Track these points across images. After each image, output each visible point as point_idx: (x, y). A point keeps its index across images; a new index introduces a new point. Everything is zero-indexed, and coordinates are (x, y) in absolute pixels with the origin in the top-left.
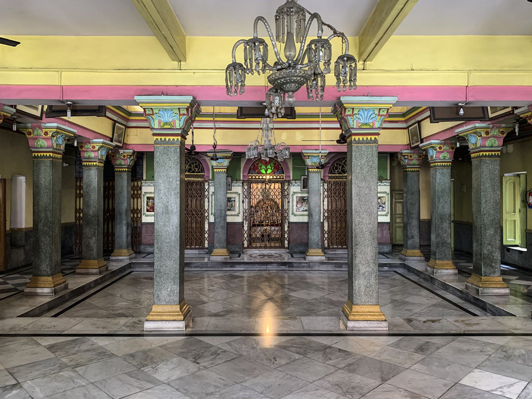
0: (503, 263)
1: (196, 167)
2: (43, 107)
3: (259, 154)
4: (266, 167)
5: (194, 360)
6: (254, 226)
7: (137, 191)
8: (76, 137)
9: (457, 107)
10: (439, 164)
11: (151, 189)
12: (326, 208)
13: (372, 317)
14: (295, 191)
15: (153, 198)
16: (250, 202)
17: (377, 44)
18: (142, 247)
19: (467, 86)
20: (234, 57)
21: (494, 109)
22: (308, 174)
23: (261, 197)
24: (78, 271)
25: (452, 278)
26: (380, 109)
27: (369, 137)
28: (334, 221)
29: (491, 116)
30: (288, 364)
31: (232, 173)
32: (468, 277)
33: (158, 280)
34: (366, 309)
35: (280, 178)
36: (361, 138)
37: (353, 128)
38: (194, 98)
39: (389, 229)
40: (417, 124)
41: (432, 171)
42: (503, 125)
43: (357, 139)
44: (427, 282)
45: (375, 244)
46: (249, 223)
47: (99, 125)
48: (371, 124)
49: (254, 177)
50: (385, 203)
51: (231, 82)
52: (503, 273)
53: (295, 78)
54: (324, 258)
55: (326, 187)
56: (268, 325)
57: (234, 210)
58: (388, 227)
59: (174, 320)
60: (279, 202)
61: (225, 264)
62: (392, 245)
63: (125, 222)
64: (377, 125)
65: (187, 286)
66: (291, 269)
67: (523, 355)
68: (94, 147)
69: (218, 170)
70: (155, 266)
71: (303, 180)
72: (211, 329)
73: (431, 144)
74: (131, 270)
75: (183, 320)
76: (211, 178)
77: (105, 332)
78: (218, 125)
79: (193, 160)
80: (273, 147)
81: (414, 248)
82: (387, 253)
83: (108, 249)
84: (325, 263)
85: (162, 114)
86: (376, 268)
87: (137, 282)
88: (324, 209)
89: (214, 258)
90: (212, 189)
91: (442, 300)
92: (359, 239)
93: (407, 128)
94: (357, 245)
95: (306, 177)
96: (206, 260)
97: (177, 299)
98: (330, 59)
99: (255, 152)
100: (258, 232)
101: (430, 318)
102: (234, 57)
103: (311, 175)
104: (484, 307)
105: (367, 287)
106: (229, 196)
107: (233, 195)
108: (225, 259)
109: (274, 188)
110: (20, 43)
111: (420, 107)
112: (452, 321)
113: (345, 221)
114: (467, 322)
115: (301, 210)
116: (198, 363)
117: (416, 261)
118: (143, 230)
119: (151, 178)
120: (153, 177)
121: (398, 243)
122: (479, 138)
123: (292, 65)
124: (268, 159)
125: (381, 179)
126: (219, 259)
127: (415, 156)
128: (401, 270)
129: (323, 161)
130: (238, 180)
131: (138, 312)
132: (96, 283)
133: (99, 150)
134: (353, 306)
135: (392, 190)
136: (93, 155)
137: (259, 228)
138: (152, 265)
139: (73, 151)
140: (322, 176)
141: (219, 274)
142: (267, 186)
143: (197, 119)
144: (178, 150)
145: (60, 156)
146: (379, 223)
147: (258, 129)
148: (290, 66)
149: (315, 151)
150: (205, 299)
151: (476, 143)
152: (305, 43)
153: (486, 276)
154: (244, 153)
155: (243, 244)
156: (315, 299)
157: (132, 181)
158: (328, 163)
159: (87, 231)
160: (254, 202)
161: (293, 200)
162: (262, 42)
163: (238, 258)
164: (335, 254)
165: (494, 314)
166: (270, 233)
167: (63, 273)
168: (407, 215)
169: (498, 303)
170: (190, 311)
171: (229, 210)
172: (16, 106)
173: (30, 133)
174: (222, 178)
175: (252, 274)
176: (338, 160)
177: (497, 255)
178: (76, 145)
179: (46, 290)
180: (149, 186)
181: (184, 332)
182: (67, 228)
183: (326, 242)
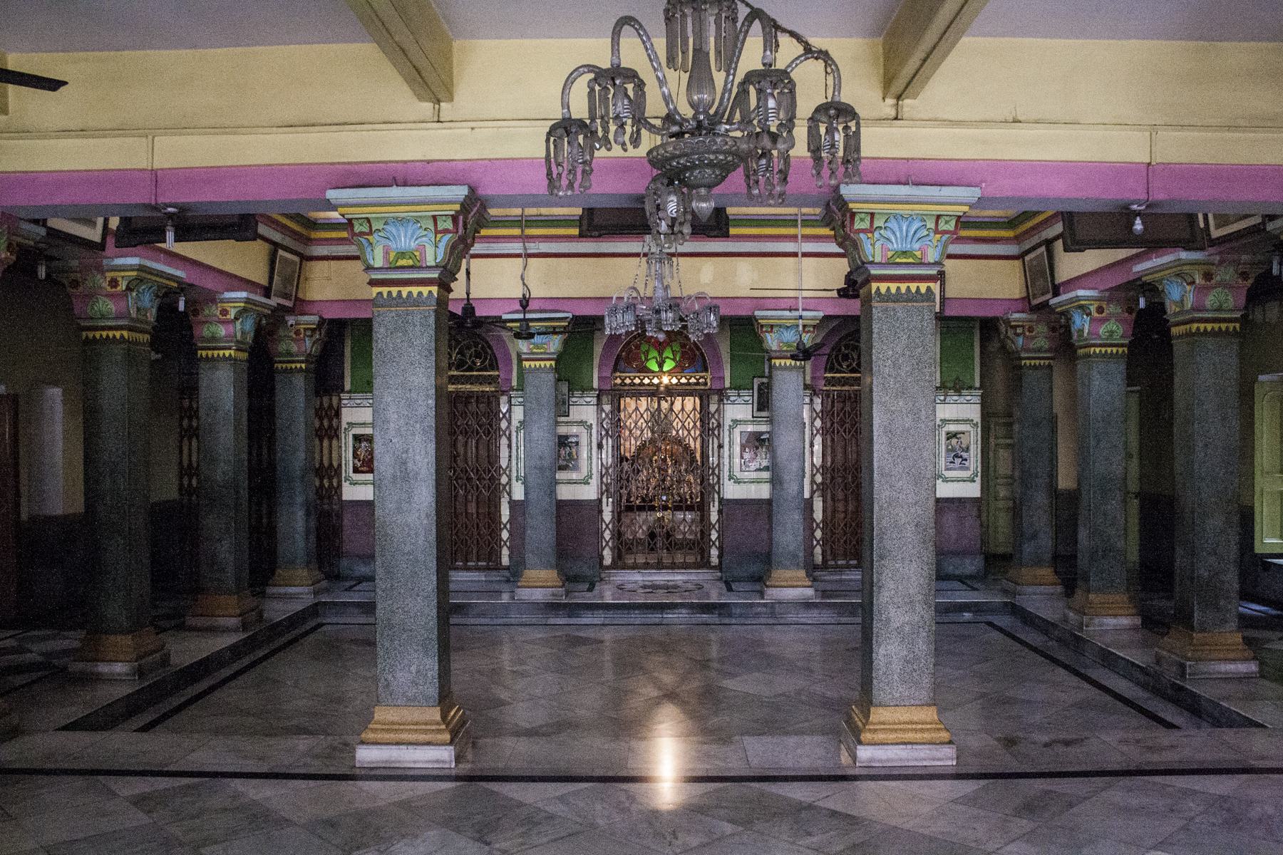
0: (1246, 596)
1: (478, 355)
2: (106, 220)
3: (641, 323)
4: (660, 354)
5: (478, 835)
6: (630, 508)
7: (330, 420)
8: (184, 288)
9: (1125, 214)
10: (1097, 350)
11: (365, 415)
12: (818, 461)
13: (919, 736)
14: (739, 417)
15: (369, 439)
16: (617, 447)
17: (925, 60)
18: (344, 563)
19: (1149, 164)
20: (565, 105)
21: (1223, 220)
22: (770, 372)
23: (648, 434)
24: (191, 621)
25: (1125, 637)
26: (938, 217)
27: (913, 286)
28: (840, 495)
29: (1215, 233)
30: (703, 845)
31: (569, 371)
32: (1163, 635)
33: (387, 644)
34: (902, 715)
35: (697, 384)
36: (893, 287)
37: (872, 263)
38: (472, 190)
39: (979, 516)
40: (1043, 249)
41: (1081, 367)
42: (1244, 257)
43: (883, 290)
44: (1067, 650)
45: (929, 555)
46: (617, 504)
47: (240, 259)
48: (918, 254)
49: (628, 381)
50: (967, 450)
51: (558, 165)
52: (1247, 622)
53: (712, 157)
54: (810, 592)
55: (818, 408)
56: (667, 762)
57: (576, 468)
58: (975, 513)
59: (428, 743)
60: (695, 445)
61: (552, 607)
62: (977, 555)
63: (299, 499)
64: (932, 256)
65: (457, 663)
66: (727, 621)
67: (1270, 817)
68: (224, 312)
69: (533, 363)
70: (380, 612)
71: (759, 389)
72: (516, 767)
73: (1078, 298)
74: (319, 620)
75: (451, 743)
76: (514, 383)
77: (265, 769)
78: (533, 247)
79: (469, 338)
80: (674, 304)
81: (1038, 563)
82: (971, 577)
83: (262, 568)
84: (815, 605)
85: (394, 231)
86: (929, 615)
87: (333, 650)
88: (813, 464)
89: (525, 594)
90: (518, 414)
91: (1097, 691)
92: (888, 543)
93: (1021, 257)
94: (882, 557)
95: (765, 380)
96: (505, 598)
97: (433, 691)
98: (793, 116)
99: (629, 318)
100: (641, 523)
101: (1063, 736)
102: (565, 105)
103: (778, 375)
104: (1196, 708)
105: (908, 662)
106: (562, 430)
107: (574, 430)
108: (553, 595)
109: (683, 409)
110: (65, 83)
111: (1038, 213)
112: (1114, 741)
113: (858, 498)
114: (1150, 744)
115: (753, 468)
116: (488, 844)
117: (1041, 597)
118: (346, 522)
119: (365, 386)
120: (370, 383)
121: (1001, 550)
122: (1188, 288)
123: (705, 126)
124: (661, 337)
125: (952, 385)
126: (538, 595)
127: (1042, 329)
128: (1004, 621)
129: (807, 339)
130: (586, 389)
131: (339, 723)
132: (235, 651)
133: (236, 319)
134: (872, 709)
135: (985, 415)
136: (222, 331)
137: (643, 515)
138: (369, 608)
139: (176, 323)
140: (808, 378)
141: (539, 634)
142: (665, 405)
143: (484, 232)
144: (432, 320)
145: (147, 337)
146: (938, 500)
147: (637, 255)
148: (700, 124)
149: (787, 313)
150: (504, 695)
151: (1182, 301)
152: (734, 75)
153: (1203, 630)
154: (601, 318)
155: (601, 558)
156: (783, 695)
157: (317, 394)
158: (818, 347)
159: (212, 522)
160: (630, 447)
161: (733, 440)
162: (632, 75)
163: (589, 594)
164: (841, 581)
165: (1217, 724)
166: (673, 529)
167: (156, 627)
168: (1023, 478)
169: (1227, 698)
170: (465, 723)
171: (561, 468)
172: (45, 221)
173: (75, 284)
174: (544, 385)
175: (624, 633)
176: (847, 335)
177: (1231, 580)
178: (181, 307)
179: (119, 668)
180: (358, 406)
181: (454, 773)
182: (160, 514)
183: (818, 550)
